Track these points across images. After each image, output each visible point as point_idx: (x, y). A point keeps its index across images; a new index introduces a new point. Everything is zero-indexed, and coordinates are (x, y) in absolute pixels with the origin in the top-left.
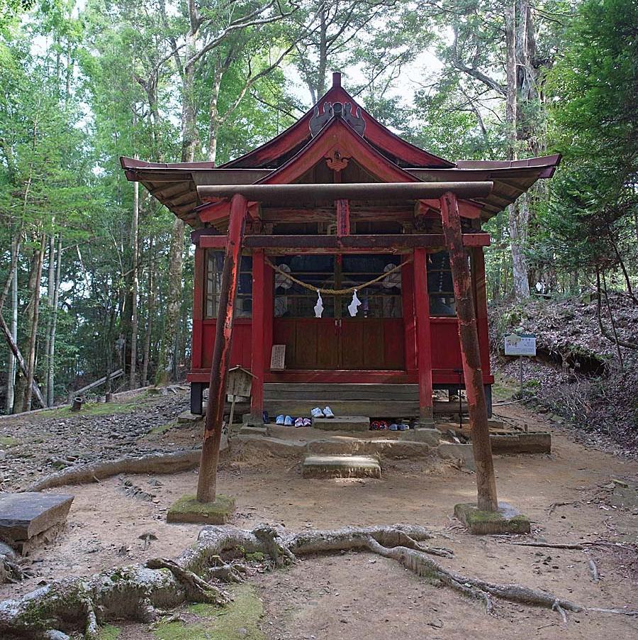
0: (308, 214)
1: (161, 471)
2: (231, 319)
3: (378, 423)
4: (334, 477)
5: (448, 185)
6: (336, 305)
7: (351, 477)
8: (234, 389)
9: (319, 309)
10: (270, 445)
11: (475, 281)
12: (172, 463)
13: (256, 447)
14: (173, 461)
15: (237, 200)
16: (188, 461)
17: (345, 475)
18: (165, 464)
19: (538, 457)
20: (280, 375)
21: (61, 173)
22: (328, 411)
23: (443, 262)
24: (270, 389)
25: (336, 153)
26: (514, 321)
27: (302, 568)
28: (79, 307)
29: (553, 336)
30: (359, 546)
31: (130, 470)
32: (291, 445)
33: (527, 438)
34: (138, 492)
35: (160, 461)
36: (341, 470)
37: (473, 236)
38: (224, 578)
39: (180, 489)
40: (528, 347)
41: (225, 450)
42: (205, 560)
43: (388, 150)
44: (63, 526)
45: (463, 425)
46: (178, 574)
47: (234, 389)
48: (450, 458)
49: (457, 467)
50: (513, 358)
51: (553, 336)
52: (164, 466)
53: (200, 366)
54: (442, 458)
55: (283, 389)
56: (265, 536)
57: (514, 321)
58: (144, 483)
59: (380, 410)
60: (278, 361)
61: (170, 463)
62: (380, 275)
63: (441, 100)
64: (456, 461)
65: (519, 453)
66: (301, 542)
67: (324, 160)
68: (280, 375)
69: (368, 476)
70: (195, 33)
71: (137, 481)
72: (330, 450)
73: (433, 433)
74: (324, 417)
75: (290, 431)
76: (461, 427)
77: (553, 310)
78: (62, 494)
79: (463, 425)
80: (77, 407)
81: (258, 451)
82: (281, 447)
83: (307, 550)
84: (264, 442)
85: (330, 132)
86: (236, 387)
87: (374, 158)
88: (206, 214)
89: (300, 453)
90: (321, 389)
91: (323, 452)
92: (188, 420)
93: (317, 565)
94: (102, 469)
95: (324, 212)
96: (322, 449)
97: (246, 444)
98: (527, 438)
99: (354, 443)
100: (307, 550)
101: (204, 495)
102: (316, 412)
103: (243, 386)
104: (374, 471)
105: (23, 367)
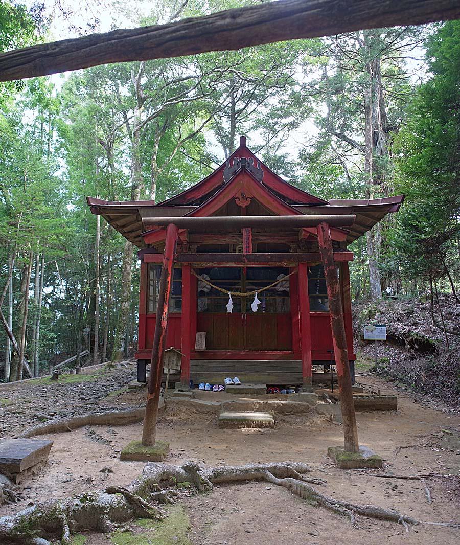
3: (273, 389)
4: (241, 428)
6: (242, 304)
7: (253, 427)
8: (169, 364)
9: (230, 307)
10: (194, 405)
12: (124, 417)
13: (185, 406)
14: (125, 416)
15: (171, 228)
18: (119, 418)
19: (388, 413)
20: (202, 354)
21: (44, 209)
22: (237, 380)
24: (195, 364)
25: (243, 194)
26: (371, 315)
27: (218, 493)
28: (57, 305)
29: (399, 326)
30: (259, 477)
31: (93, 422)
34: (99, 438)
35: (115, 416)
36: (246, 422)
37: (341, 254)
38: (161, 500)
39: (130, 436)
40: (380, 334)
42: (148, 488)
44: (45, 463)
45: (333, 390)
46: (128, 497)
47: (169, 364)
48: (325, 414)
49: (329, 420)
50: (370, 342)
51: (399, 326)
53: (144, 347)
56: (191, 470)
57: (371, 315)
58: (104, 432)
59: (274, 380)
60: (201, 344)
61: (122, 418)
63: (318, 156)
66: (217, 474)
67: (233, 199)
68: (202, 354)
69: (265, 427)
71: (99, 431)
73: (312, 396)
74: (234, 384)
75: (209, 394)
76: (332, 392)
77: (399, 308)
78: (45, 439)
79: (333, 390)
80: (55, 377)
83: (221, 480)
84: (191, 403)
85: (238, 179)
89: (216, 411)
91: (233, 410)
93: (229, 491)
96: (232, 408)
97: (177, 403)
100: (221, 480)
101: (147, 441)
102: (228, 381)
103: (175, 362)
104: (269, 423)
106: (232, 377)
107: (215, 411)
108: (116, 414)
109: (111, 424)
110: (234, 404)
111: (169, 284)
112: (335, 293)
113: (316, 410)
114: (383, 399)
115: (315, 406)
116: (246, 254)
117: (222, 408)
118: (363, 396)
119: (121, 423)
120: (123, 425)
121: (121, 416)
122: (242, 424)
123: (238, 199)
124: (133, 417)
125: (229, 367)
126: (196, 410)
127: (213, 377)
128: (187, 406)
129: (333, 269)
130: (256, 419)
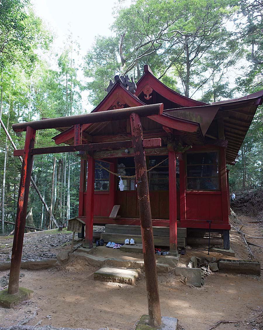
0: (113, 137)
1: (33, 268)
2: (23, 195)
4: (108, 281)
5: (133, 108)
7: (117, 282)
8: (73, 229)
10: (87, 259)
11: (220, 170)
12: (38, 265)
13: (81, 259)
14: (39, 264)
16: (47, 264)
17: (114, 281)
18: (35, 265)
19: (251, 277)
22: (132, 241)
23: (203, 160)
24: (110, 227)
25: (118, 103)
32: (97, 260)
33: (245, 264)
35: (33, 263)
36: (111, 277)
37: (149, 140)
41: (65, 260)
43: (174, 102)
45: (210, 253)
47: (73, 229)
48: (180, 276)
49: (183, 281)
52: (34, 266)
53: (82, 214)
54: (176, 275)
55: (116, 228)
60: (114, 214)
61: (37, 265)
62: (151, 168)
63: (250, 81)
64: (183, 278)
65: (239, 273)
69: (126, 283)
70: (123, 65)
72: (116, 264)
73: (174, 260)
74: (129, 244)
76: (208, 254)
79: (210, 253)
81: (82, 262)
82: (92, 261)
84: (85, 257)
85: (115, 91)
86: (75, 228)
87: (137, 103)
88: (58, 140)
90: (134, 229)
91: (112, 265)
92: (76, 240)
94: (4, 266)
95: (121, 136)
96: (112, 264)
97: (76, 257)
98: (245, 264)
99: (128, 262)
103: (78, 228)
104: (129, 280)
105: (48, 211)
106: (129, 238)
107: (101, 265)
108: (33, 262)
109: (29, 269)
110: (113, 261)
111: (26, 172)
112: (139, 176)
113: (175, 272)
114: (247, 265)
115: (174, 268)
116: (76, 145)
117: (106, 264)
118: (230, 261)
119: (36, 269)
120: (37, 270)
121: (36, 264)
122: (110, 279)
123: (115, 107)
124: (45, 265)
125: (132, 231)
126: (88, 263)
127: (118, 238)
128: (83, 260)
129: (139, 154)
130: (119, 276)
